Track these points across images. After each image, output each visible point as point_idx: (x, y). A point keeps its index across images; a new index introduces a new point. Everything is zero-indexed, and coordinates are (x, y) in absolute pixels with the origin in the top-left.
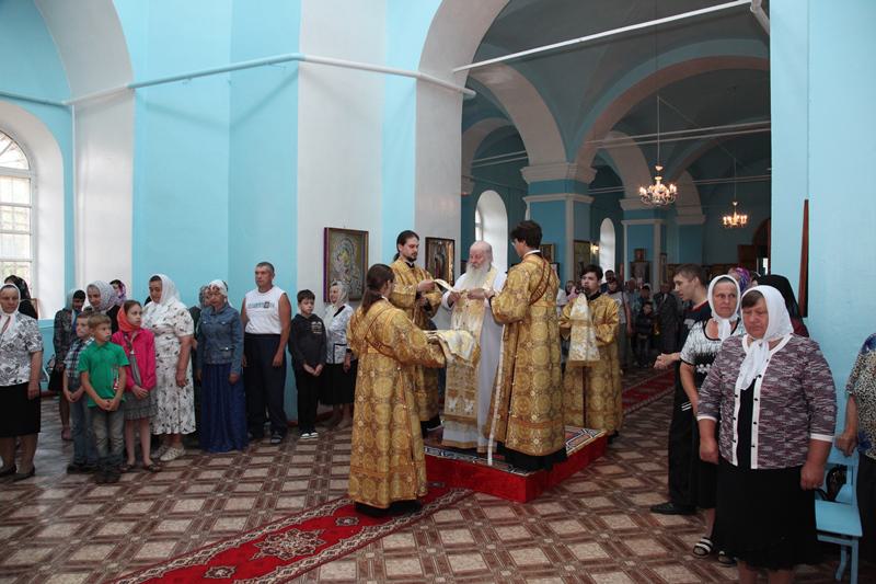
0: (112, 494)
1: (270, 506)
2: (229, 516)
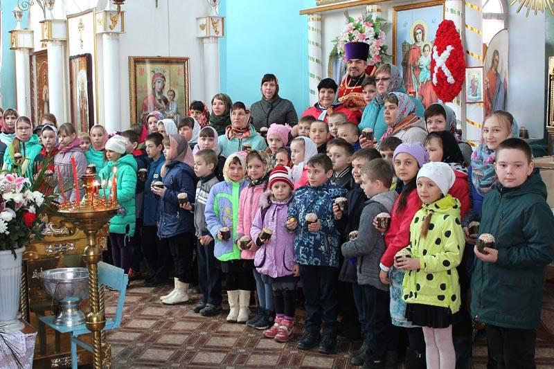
0: (132, 339)
1: (213, 328)
2: (173, 333)
